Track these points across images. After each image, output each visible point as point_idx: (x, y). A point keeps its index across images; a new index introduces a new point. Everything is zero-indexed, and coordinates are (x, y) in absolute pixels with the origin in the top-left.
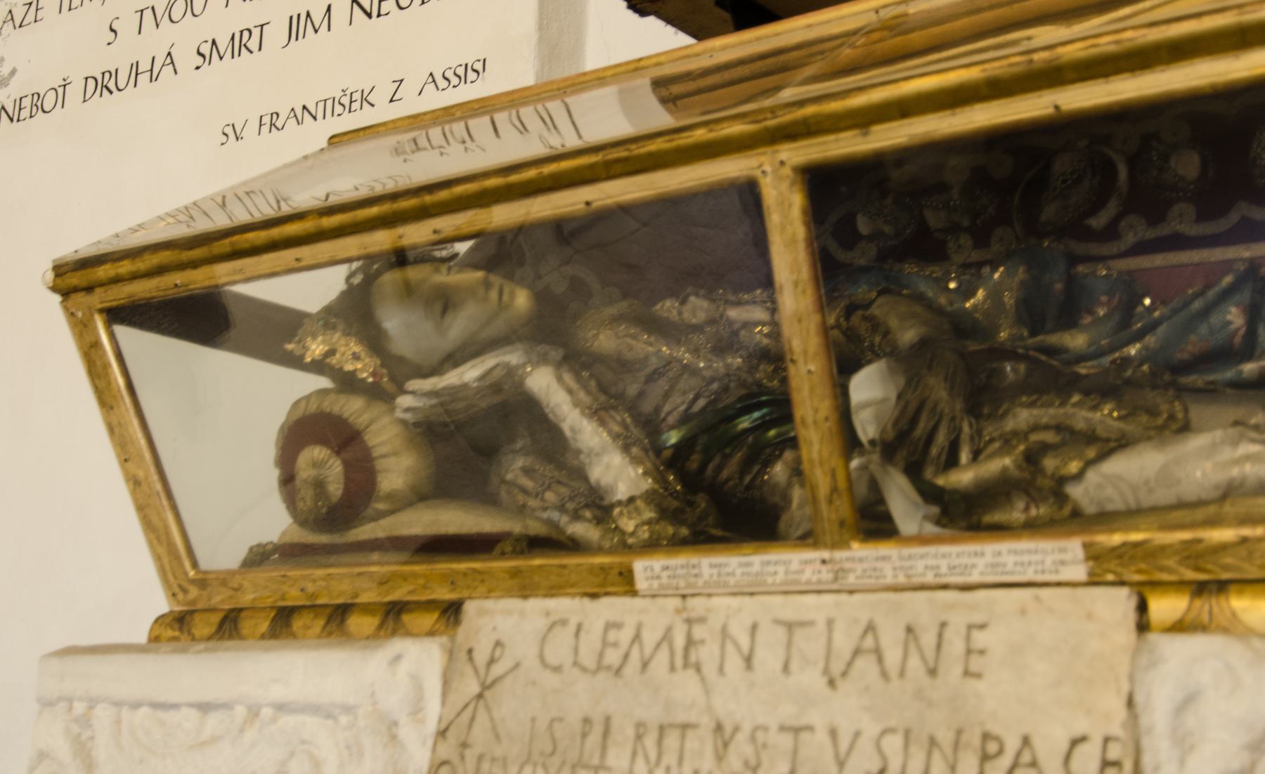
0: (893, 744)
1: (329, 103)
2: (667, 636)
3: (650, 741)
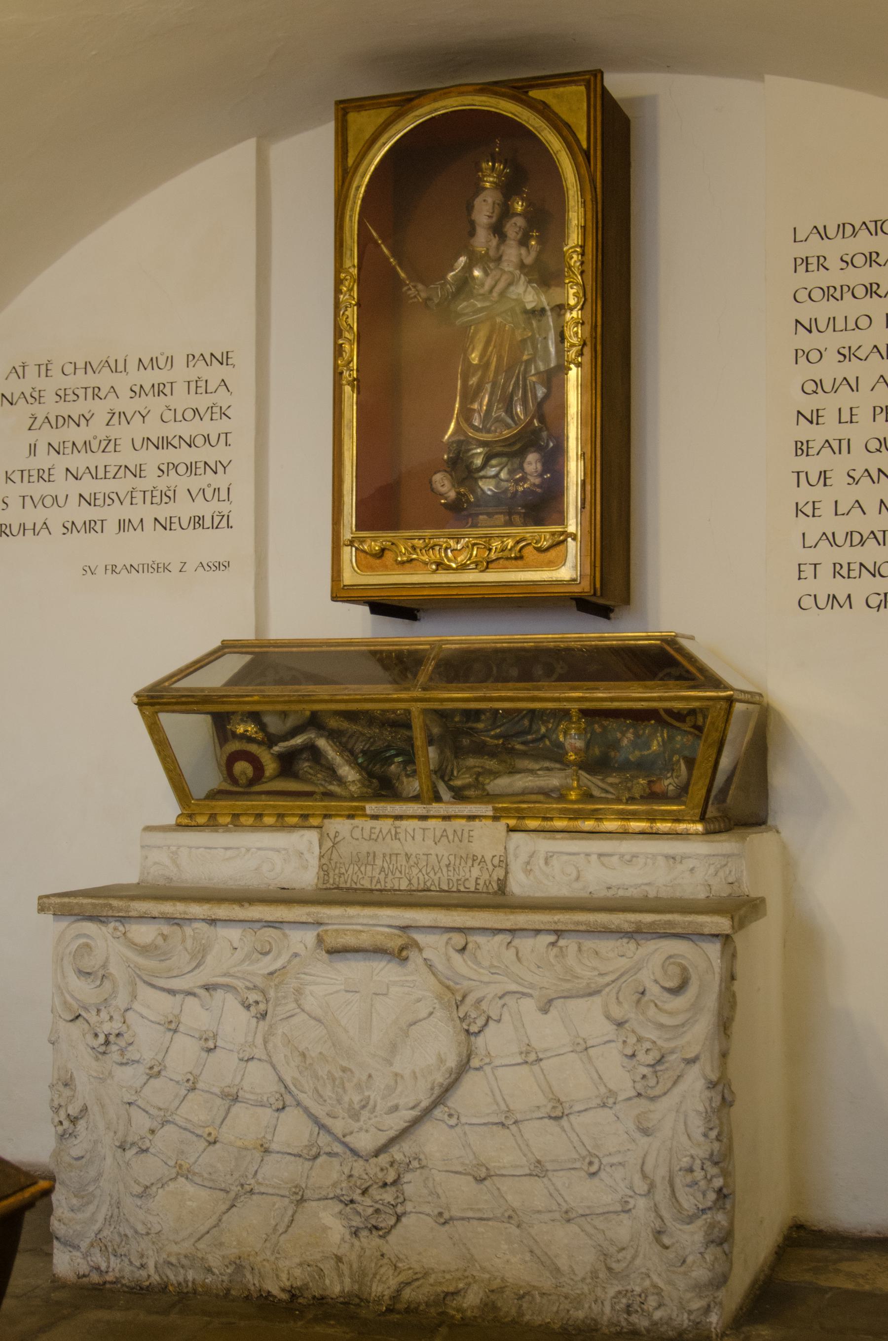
0: (452, 858)
1: (146, 566)
2: (390, 831)
3: (388, 858)
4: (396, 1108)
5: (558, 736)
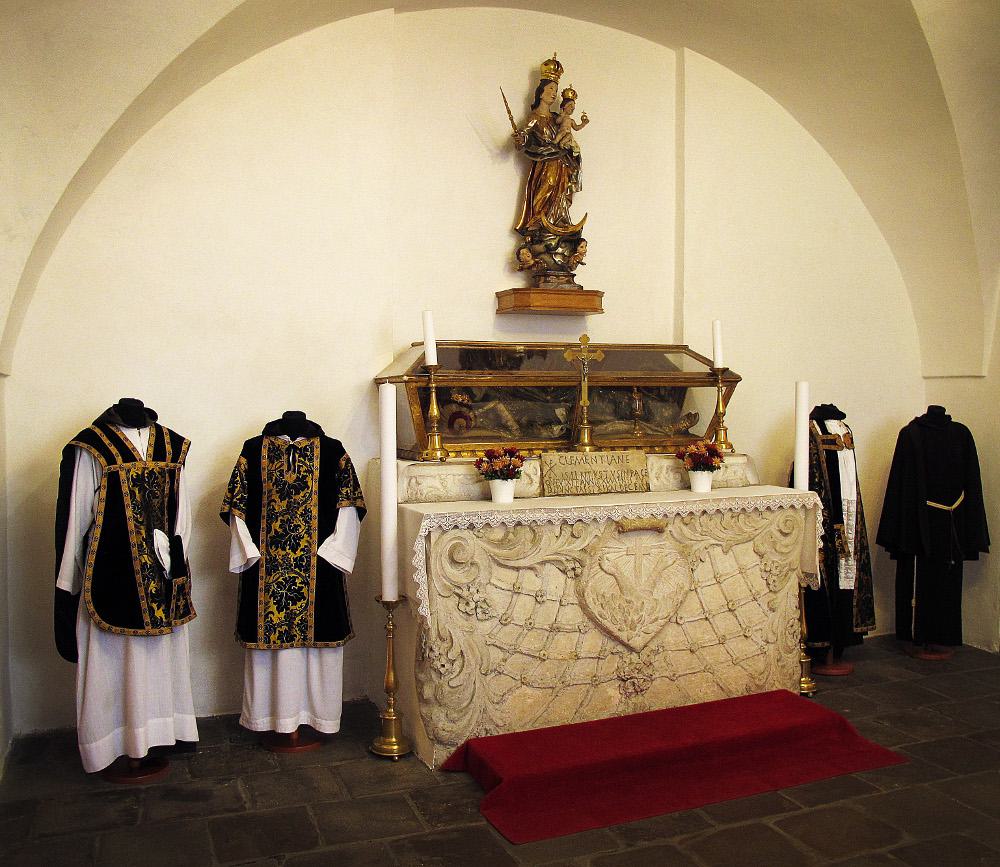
4: (656, 619)
5: (515, 414)
